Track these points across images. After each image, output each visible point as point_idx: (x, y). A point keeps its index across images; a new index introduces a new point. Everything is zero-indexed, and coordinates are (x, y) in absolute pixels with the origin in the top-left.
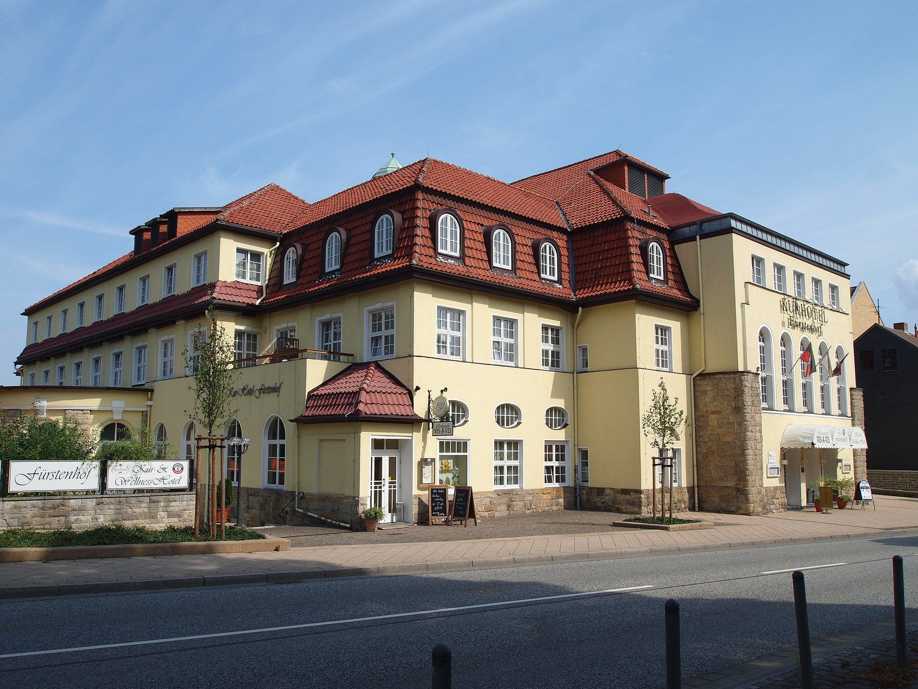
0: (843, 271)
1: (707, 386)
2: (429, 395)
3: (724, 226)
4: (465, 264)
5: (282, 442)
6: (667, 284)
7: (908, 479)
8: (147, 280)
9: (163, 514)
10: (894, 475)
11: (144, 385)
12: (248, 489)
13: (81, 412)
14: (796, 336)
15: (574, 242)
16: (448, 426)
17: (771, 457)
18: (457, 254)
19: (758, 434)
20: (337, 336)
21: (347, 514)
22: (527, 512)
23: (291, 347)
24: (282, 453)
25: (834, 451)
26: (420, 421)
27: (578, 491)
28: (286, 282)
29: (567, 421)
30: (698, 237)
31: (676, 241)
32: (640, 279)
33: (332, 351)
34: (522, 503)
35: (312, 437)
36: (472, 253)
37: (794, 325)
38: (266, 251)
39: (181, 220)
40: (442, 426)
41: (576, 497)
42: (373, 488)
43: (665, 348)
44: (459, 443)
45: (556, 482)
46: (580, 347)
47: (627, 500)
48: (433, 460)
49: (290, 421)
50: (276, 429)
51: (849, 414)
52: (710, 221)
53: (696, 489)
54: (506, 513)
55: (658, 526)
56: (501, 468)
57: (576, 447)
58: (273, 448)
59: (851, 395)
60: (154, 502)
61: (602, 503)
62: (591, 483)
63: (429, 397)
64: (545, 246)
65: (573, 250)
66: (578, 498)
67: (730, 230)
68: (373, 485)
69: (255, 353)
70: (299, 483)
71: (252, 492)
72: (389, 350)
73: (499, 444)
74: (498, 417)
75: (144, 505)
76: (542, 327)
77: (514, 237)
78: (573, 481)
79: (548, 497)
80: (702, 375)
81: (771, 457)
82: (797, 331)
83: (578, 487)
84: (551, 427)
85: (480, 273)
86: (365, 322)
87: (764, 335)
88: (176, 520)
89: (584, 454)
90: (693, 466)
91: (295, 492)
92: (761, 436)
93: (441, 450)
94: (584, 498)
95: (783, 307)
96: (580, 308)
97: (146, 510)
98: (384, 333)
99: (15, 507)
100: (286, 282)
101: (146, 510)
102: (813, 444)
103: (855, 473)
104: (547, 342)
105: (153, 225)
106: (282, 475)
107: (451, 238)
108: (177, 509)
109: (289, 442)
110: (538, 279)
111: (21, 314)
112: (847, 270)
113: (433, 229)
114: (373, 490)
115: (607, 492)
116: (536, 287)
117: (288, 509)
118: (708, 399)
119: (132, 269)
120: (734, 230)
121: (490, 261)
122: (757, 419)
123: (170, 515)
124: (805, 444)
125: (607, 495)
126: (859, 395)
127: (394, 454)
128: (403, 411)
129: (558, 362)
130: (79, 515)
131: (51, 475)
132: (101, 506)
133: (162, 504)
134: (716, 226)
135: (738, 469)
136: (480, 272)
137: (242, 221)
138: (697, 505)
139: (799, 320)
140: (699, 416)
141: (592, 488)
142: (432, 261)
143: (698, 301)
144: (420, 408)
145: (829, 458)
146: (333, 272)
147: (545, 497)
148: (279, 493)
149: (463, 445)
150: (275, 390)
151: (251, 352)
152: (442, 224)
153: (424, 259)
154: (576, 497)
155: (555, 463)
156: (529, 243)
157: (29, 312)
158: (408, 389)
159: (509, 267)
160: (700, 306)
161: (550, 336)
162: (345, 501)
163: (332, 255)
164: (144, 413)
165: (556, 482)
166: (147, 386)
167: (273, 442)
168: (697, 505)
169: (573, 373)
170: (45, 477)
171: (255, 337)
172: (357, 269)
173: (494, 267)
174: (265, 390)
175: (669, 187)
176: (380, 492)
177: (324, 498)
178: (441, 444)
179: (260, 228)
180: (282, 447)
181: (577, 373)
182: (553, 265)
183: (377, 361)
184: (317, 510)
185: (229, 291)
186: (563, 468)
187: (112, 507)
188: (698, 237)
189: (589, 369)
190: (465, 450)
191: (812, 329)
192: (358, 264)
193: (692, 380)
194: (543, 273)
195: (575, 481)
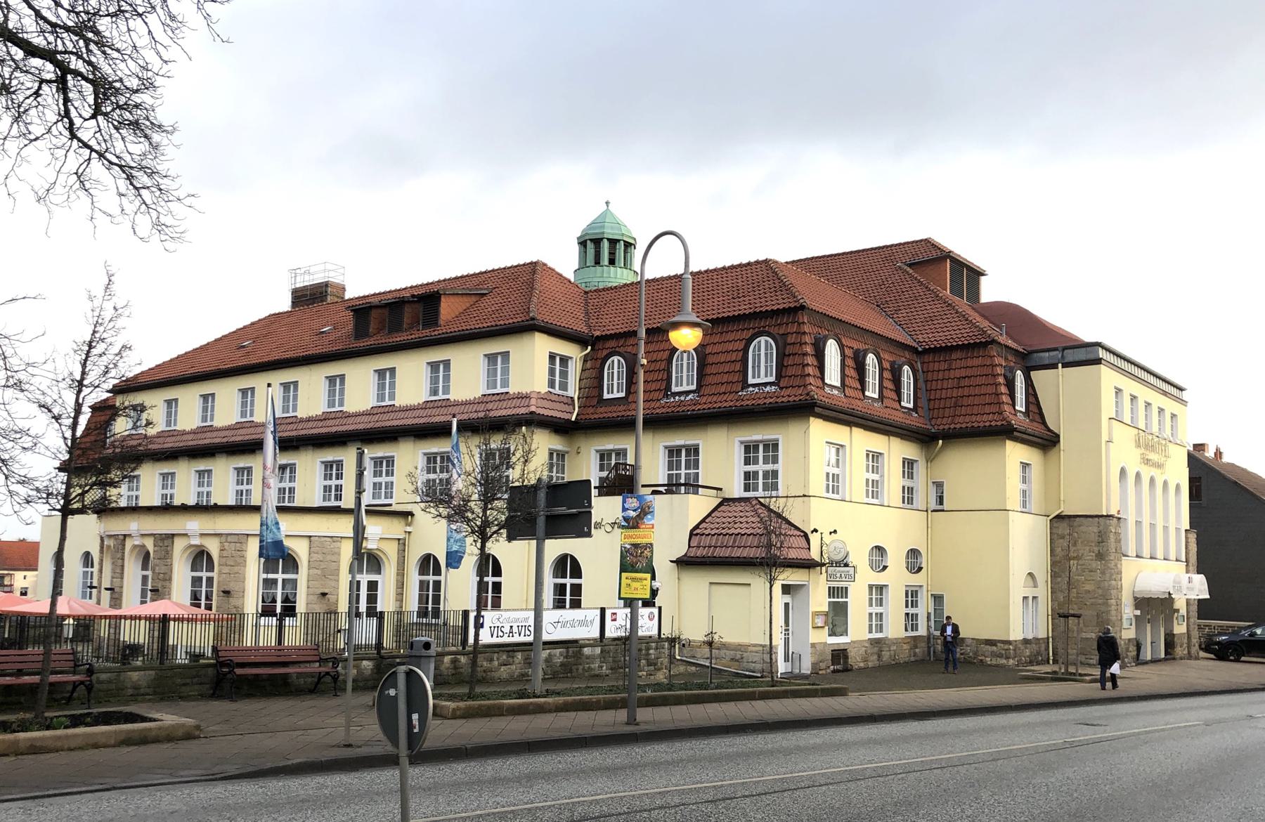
1: (1063, 528)
13: (329, 539)
14: (1147, 473)
16: (848, 572)
19: (1119, 583)
29: (921, 563)
30: (1060, 365)
34: (888, 653)
37: (1147, 462)
40: (839, 571)
41: (929, 648)
46: (933, 483)
47: (992, 652)
49: (671, 561)
51: (1184, 560)
53: (1051, 640)
54: (877, 663)
55: (743, 693)
59: (1187, 538)
61: (962, 654)
67: (1098, 361)
72: (775, 487)
76: (904, 462)
77: (844, 350)
80: (1059, 517)
87: (1123, 472)
96: (941, 442)
102: (1170, 594)
110: (862, 397)
112: (1185, 395)
120: (1103, 362)
126: (1193, 537)
128: (802, 555)
134: (1081, 355)
135: (1100, 620)
140: (1056, 562)
143: (1058, 436)
148: (915, 638)
160: (1059, 441)
164: (401, 542)
168: (1051, 658)
169: (927, 511)
175: (990, 292)
189: (946, 507)
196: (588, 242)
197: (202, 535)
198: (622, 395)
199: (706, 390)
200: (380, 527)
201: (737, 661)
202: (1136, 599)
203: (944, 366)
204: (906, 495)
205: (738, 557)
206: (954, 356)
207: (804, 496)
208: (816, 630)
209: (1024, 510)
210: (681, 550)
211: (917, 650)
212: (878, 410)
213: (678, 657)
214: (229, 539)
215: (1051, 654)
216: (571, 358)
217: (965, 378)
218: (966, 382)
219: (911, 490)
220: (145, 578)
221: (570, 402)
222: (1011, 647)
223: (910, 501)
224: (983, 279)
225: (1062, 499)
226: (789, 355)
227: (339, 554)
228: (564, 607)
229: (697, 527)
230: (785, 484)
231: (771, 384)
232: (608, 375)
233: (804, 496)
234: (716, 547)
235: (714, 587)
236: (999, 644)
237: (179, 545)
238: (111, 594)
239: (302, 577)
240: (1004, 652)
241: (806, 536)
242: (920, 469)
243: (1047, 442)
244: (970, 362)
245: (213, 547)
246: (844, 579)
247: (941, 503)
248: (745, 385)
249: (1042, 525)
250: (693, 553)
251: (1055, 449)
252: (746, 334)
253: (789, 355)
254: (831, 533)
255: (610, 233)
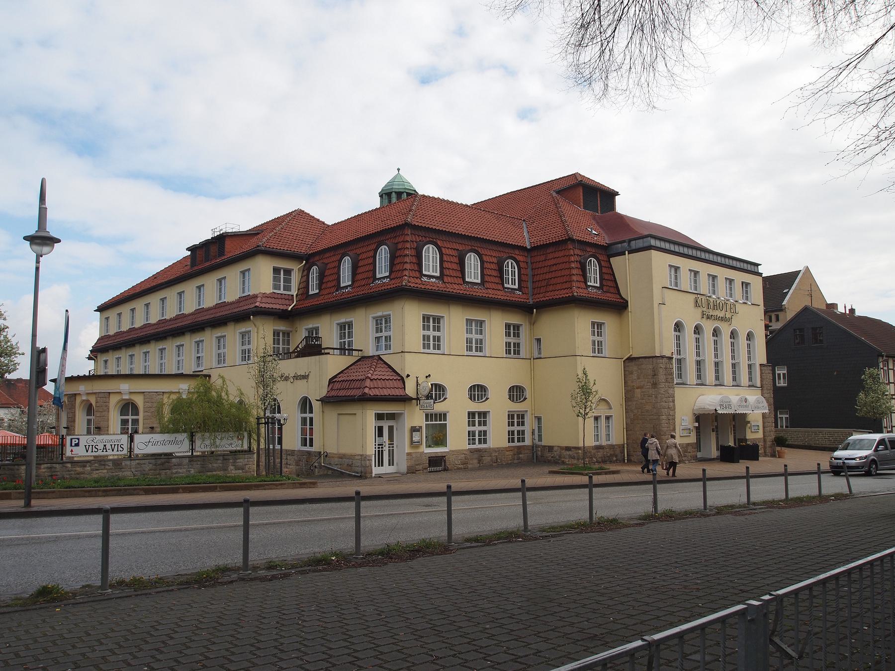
0: (756, 271)
1: (633, 367)
2: (417, 380)
3: (646, 245)
4: (443, 281)
5: (311, 415)
6: (603, 290)
7: (827, 436)
8: (202, 288)
9: (232, 467)
10: (816, 432)
11: (202, 371)
12: (287, 450)
13: (155, 393)
15: (532, 257)
17: (684, 420)
18: (438, 274)
19: (671, 404)
20: (350, 335)
21: (358, 467)
22: (494, 464)
23: (316, 343)
24: (311, 424)
25: (744, 416)
26: (411, 399)
27: (535, 448)
28: (311, 293)
31: (612, 254)
32: (579, 288)
33: (347, 351)
34: (489, 458)
35: (332, 414)
36: (450, 273)
38: (296, 268)
39: (228, 243)
40: (426, 403)
41: (533, 454)
42: (377, 448)
43: (600, 338)
44: (440, 415)
45: (278, 444)
46: (536, 339)
48: (421, 427)
49: (317, 400)
50: (305, 404)
51: (759, 384)
52: (635, 240)
53: (626, 446)
55: (577, 473)
56: (513, 432)
57: (533, 415)
58: (304, 420)
60: (226, 459)
61: (552, 457)
62: (544, 443)
63: (417, 382)
64: (508, 263)
65: (531, 263)
66: (535, 454)
68: (377, 446)
69: (288, 347)
70: (324, 445)
71: (292, 453)
72: (388, 347)
73: (471, 415)
74: (471, 394)
75: (219, 461)
76: (506, 325)
78: (531, 441)
79: (511, 453)
80: (630, 359)
81: (684, 420)
82: (709, 322)
83: (535, 445)
84: (513, 401)
85: (456, 288)
86: (370, 327)
87: (678, 327)
88: (241, 471)
89: (539, 419)
90: (624, 428)
91: (321, 452)
92: (674, 405)
93: (427, 420)
94: (539, 453)
95: (696, 304)
96: (535, 310)
97: (221, 465)
98: (384, 334)
99: (138, 464)
100: (311, 293)
101: (221, 465)
102: (716, 410)
103: (764, 432)
104: (509, 336)
105: (206, 244)
106: (311, 440)
107: (433, 262)
108: (241, 464)
109: (317, 414)
111: (94, 311)
113: (419, 256)
114: (377, 449)
115: (555, 449)
116: (500, 295)
117: (316, 464)
118: (635, 376)
119: (189, 279)
121: (463, 277)
122: (670, 391)
123: (237, 468)
124: (710, 410)
125: (556, 451)
127: (391, 423)
129: (519, 351)
130: (178, 469)
131: (159, 443)
132: (192, 463)
133: (231, 461)
134: (640, 244)
136: (456, 286)
137: (275, 245)
138: (626, 458)
139: (711, 313)
141: (545, 446)
142: (418, 281)
144: (410, 390)
145: (738, 421)
146: (346, 287)
147: (508, 453)
148: (309, 453)
149: (443, 416)
150: (305, 377)
151: (286, 346)
152: (425, 253)
153: (412, 280)
154: (533, 454)
155: (516, 428)
156: (495, 260)
157: (101, 309)
158: (401, 377)
159: (479, 281)
160: (628, 306)
161: (512, 331)
162: (357, 457)
163: (345, 274)
165: (278, 444)
166: (205, 372)
167: (304, 415)
168: (626, 458)
170: (156, 444)
171: (288, 334)
172: (364, 285)
173: (466, 282)
174: (297, 377)
176: (382, 451)
177: (342, 456)
178: (427, 415)
179: (291, 250)
180: (311, 419)
181: (534, 359)
182: (515, 276)
183: (379, 355)
184: (337, 465)
185: (269, 300)
186: (523, 432)
187: (199, 463)
188: (627, 252)
190: (445, 420)
191: (723, 319)
192: (364, 282)
193: (623, 362)
194: (506, 283)
195: (533, 441)
196: (394, 193)
197: (88, 394)
198: (317, 291)
199: (356, 284)
200: (84, 386)
201: (350, 466)
202: (695, 414)
203: (543, 258)
204: (597, 347)
205: (349, 396)
206: (548, 251)
207: (402, 352)
208: (682, 438)
209: (594, 355)
210: (324, 393)
211: (520, 456)
212: (480, 292)
213: (323, 464)
214: (100, 395)
215: (626, 456)
216: (293, 269)
217: (554, 265)
218: (554, 268)
219: (600, 343)
220: (89, 421)
221: (290, 298)
222: (580, 451)
223: (517, 352)
224: (617, 197)
225: (631, 346)
226: (398, 257)
227: (674, 397)
228: (520, 426)
229: (335, 377)
230: (395, 346)
231: (386, 277)
232: (343, 278)
233: (402, 352)
234: (340, 390)
235: (340, 416)
236: (572, 450)
237: (114, 400)
238: (67, 431)
239: (141, 417)
240: (576, 455)
241: (402, 379)
242: (524, 331)
243: (619, 306)
244: (557, 254)
245: (139, 401)
246: (428, 408)
247: (540, 353)
248: (375, 279)
249: (620, 363)
250: (333, 393)
251: (626, 312)
252: (374, 246)
253: (398, 257)
254: (430, 375)
255: (396, 187)
